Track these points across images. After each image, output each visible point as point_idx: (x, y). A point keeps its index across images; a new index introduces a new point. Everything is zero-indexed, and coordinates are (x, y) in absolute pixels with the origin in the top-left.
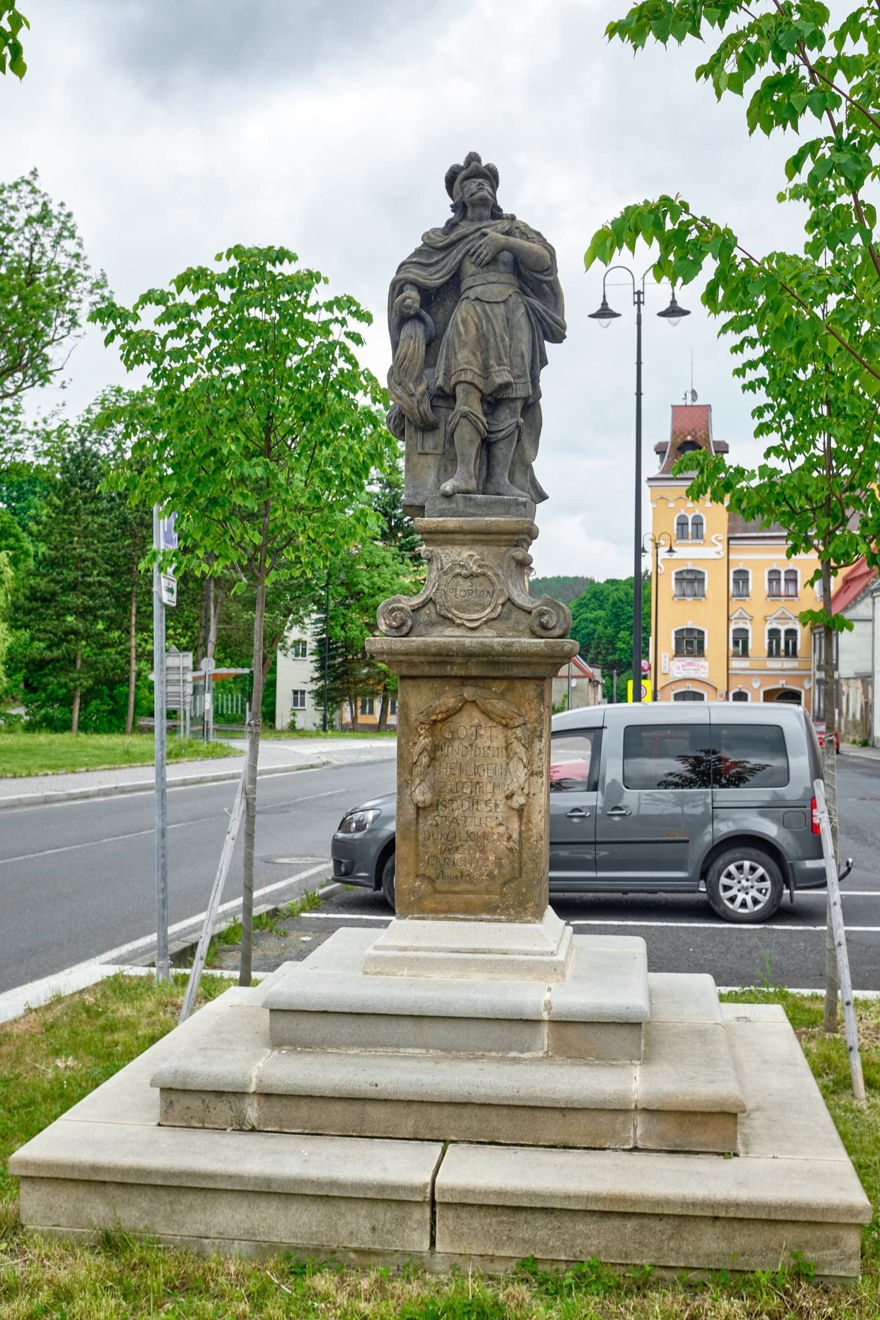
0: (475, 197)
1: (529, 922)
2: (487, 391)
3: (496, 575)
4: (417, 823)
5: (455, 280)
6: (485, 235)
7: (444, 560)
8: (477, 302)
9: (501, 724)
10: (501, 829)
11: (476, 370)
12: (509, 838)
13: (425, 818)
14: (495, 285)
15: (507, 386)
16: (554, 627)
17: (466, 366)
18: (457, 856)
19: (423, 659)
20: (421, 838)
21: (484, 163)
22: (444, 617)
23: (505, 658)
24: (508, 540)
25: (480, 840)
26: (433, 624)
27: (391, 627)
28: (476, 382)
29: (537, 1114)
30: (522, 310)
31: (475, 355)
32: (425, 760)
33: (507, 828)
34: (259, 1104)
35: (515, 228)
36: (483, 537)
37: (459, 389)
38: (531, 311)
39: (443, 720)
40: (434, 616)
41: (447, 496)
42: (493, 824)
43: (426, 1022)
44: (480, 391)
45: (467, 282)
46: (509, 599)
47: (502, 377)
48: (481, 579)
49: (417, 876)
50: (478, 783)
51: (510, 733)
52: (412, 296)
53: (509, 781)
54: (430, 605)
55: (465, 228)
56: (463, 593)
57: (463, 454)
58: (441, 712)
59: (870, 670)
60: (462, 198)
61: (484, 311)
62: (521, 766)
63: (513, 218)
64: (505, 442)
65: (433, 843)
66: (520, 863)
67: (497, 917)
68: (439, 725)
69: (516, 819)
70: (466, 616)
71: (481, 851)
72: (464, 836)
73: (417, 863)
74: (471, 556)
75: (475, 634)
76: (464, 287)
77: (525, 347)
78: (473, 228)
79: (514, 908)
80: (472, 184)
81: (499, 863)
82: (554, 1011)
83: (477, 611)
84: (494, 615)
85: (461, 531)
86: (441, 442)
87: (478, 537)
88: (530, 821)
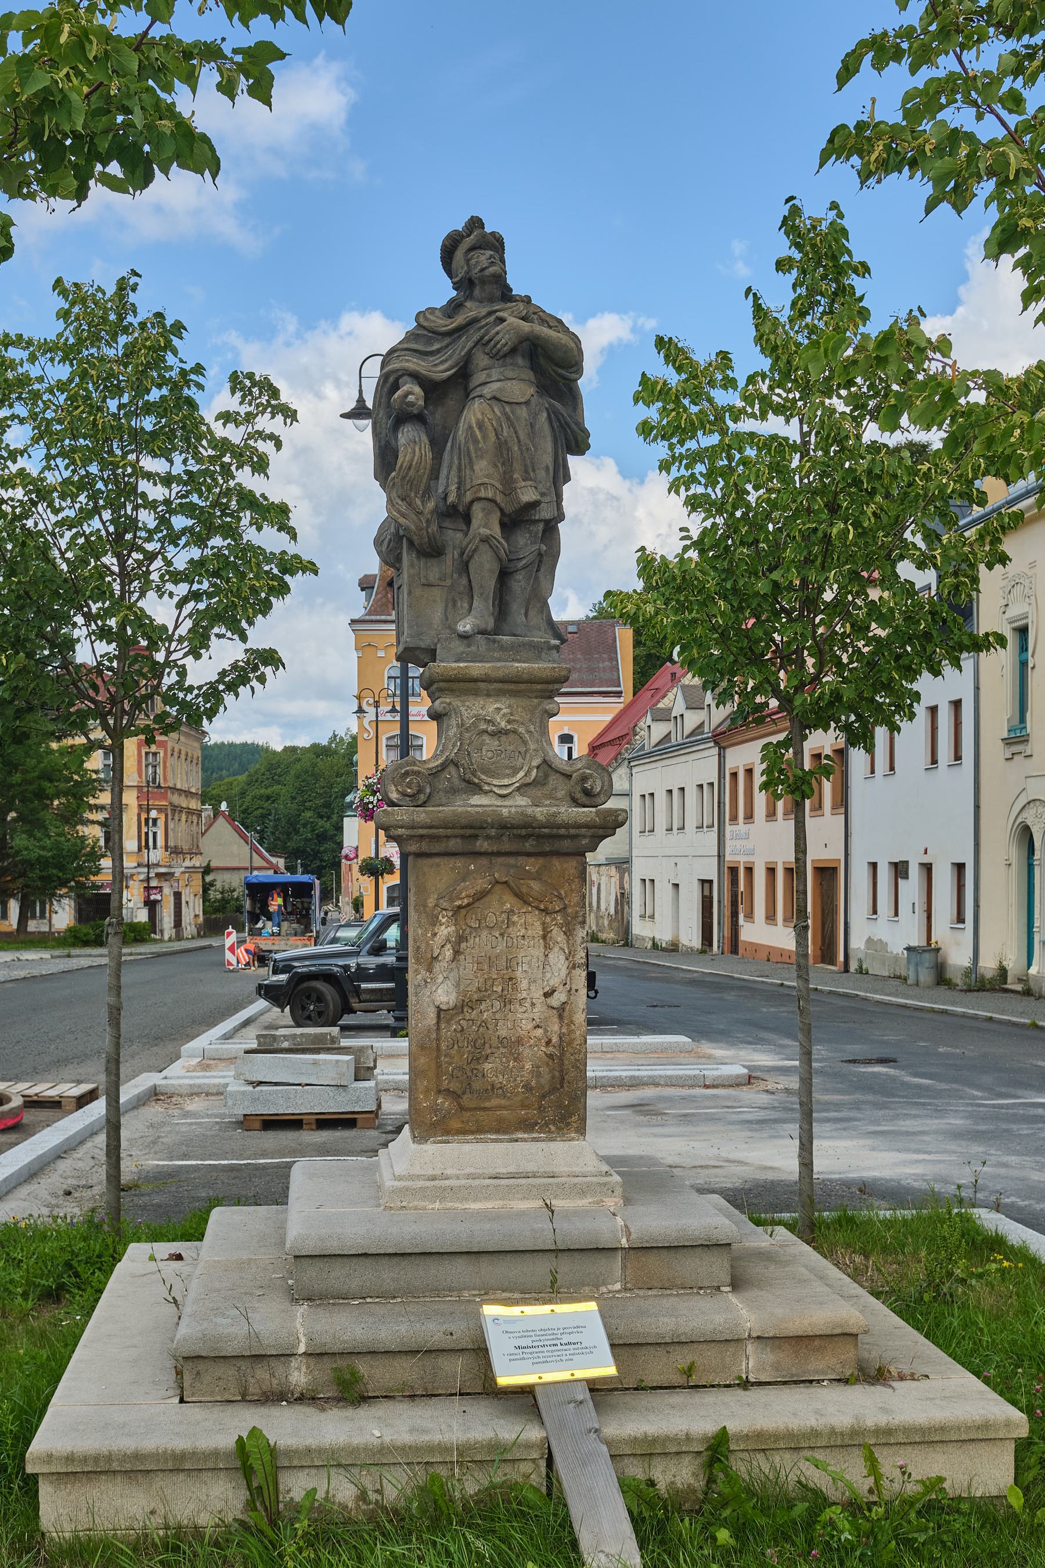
0: (487, 273)
1: (573, 1139)
2: (509, 509)
3: (529, 732)
4: (438, 1029)
5: (463, 374)
6: (502, 320)
7: (465, 714)
8: (493, 402)
9: (537, 908)
10: (539, 1032)
11: (498, 485)
12: (548, 1043)
13: (448, 1022)
14: (514, 382)
15: (534, 505)
16: (599, 794)
17: (486, 480)
18: (487, 1066)
19: (449, 832)
20: (443, 1046)
21: (488, 229)
22: (469, 782)
23: (546, 831)
24: (542, 691)
25: (513, 1045)
26: (453, 791)
27: (404, 794)
28: (498, 499)
29: (637, 1351)
30: (545, 415)
31: (496, 466)
32: (448, 953)
33: (546, 1031)
34: (308, 1368)
35: (530, 311)
36: (512, 687)
37: (477, 508)
38: (554, 416)
39: (468, 905)
40: (456, 782)
41: (464, 637)
42: (530, 1026)
43: (484, 1260)
44: (501, 510)
45: (480, 377)
46: (545, 761)
47: (528, 495)
48: (512, 736)
49: (439, 1092)
50: (511, 979)
51: (548, 919)
52: (412, 393)
53: (548, 975)
54: (452, 769)
55: (472, 310)
56: (490, 754)
57: (481, 587)
58: (468, 896)
59: (626, 855)
60: (467, 273)
61: (505, 414)
62: (562, 957)
63: (527, 300)
64: (523, 572)
65: (459, 1051)
66: (561, 1071)
67: (535, 1135)
68: (463, 912)
69: (556, 1020)
70: (495, 782)
71: (515, 1060)
72: (495, 1042)
73: (438, 1077)
74: (499, 709)
75: (506, 803)
76: (472, 385)
77: (548, 459)
78: (484, 311)
79: (554, 1124)
80: (473, 256)
81: (536, 1072)
82: (633, 1236)
83: (508, 776)
84: (528, 780)
85: (487, 679)
86: (449, 571)
87: (506, 686)
88: (572, 1022)
